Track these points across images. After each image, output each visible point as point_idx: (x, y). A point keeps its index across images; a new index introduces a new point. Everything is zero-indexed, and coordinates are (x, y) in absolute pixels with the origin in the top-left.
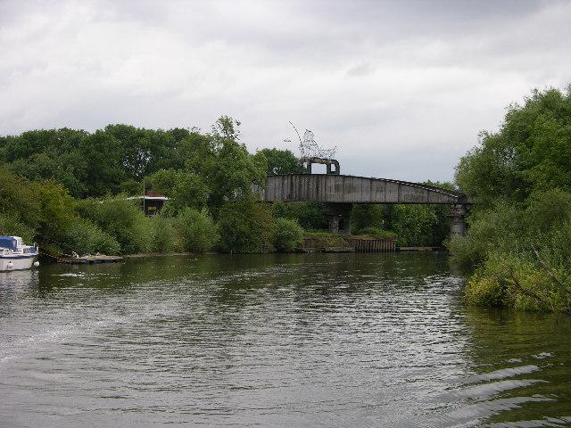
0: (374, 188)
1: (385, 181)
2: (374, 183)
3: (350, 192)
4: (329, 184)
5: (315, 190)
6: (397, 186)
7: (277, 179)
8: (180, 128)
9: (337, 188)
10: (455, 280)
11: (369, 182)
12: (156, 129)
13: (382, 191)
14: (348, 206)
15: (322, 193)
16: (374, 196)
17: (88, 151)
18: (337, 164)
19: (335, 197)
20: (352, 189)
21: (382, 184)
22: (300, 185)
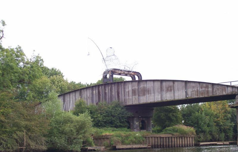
0: (165, 89)
1: (174, 81)
2: (164, 84)
3: (144, 95)
4: (127, 90)
5: (116, 96)
6: (184, 84)
7: (88, 91)
8: (48, 64)
9: (134, 92)
10: (169, 115)
11: (159, 83)
12: (77, 82)
13: (171, 90)
14: (149, 107)
15: (122, 97)
16: (164, 96)
17: (198, 111)
18: (139, 74)
19: (133, 100)
20: (145, 92)
21: (171, 84)
22: (105, 93)
